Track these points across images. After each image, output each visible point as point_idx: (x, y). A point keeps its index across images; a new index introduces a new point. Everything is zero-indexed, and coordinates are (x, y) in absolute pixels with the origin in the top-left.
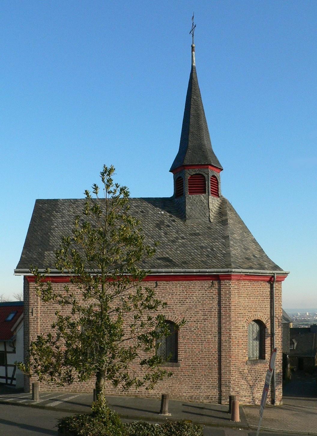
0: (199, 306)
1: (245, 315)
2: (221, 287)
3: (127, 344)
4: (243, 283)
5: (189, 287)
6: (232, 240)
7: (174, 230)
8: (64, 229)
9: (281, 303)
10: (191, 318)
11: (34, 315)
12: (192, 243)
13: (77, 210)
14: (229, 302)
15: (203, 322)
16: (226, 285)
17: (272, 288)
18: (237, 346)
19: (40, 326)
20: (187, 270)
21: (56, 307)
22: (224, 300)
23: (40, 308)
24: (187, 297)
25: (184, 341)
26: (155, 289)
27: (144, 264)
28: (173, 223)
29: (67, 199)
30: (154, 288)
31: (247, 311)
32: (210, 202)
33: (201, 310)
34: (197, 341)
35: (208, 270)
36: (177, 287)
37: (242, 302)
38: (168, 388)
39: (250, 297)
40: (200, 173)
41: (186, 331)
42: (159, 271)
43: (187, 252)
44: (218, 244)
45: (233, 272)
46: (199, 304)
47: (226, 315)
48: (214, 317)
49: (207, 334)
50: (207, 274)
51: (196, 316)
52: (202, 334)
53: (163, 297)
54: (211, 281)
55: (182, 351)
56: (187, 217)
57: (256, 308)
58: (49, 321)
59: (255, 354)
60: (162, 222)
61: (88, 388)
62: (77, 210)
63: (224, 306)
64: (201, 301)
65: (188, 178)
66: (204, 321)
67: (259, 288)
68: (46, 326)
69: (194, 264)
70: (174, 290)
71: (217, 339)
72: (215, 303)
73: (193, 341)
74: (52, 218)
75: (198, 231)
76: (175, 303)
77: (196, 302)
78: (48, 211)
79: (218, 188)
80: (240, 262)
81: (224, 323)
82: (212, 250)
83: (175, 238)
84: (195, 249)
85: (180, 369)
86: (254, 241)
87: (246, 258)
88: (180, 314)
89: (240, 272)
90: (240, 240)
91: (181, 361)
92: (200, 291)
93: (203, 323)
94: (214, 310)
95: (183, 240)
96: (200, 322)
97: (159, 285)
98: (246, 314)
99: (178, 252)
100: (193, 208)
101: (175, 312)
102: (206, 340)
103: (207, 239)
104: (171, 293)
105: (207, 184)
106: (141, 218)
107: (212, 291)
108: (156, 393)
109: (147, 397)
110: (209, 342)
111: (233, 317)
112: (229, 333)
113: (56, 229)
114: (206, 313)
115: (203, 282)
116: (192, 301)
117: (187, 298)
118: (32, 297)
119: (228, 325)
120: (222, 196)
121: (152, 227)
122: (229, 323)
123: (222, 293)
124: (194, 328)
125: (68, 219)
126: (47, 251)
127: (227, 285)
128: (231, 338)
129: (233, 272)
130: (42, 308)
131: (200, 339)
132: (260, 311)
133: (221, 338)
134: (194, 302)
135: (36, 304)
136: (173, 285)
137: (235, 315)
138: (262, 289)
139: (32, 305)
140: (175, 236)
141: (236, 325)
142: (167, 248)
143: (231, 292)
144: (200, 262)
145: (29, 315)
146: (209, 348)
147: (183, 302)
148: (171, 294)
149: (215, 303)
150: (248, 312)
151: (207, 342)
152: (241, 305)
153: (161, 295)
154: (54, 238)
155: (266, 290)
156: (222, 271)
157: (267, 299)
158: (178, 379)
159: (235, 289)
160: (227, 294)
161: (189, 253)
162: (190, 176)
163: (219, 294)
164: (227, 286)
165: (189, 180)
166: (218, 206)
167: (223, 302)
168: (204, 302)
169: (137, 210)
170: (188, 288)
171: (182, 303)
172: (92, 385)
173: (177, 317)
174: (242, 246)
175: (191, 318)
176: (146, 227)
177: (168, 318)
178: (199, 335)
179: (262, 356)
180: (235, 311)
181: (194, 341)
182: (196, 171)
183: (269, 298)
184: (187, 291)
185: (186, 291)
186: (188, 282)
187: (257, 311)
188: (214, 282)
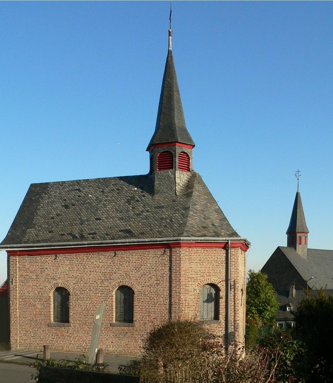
0: (152, 272)
1: (197, 280)
2: (172, 254)
3: (90, 307)
4: (195, 250)
5: (144, 255)
6: (192, 211)
7: (141, 205)
8: (48, 209)
9: (237, 267)
10: (145, 283)
11: (13, 285)
12: (155, 215)
13: (62, 191)
14: (179, 267)
15: (156, 286)
16: (177, 252)
17: (227, 254)
18: (187, 308)
19: (19, 294)
20: (140, 240)
21: (31, 277)
22: (175, 266)
23: (19, 278)
24: (142, 264)
25: (139, 304)
26: (114, 258)
27: (106, 237)
28: (143, 198)
29: (57, 182)
30: (113, 257)
31: (200, 275)
32: (176, 177)
33: (154, 275)
34: (151, 303)
35: (159, 239)
36: (133, 256)
37: (194, 268)
38: (124, 346)
39: (202, 262)
40: (169, 150)
41: (140, 295)
42: (116, 242)
43: (148, 224)
44: (178, 215)
45: (183, 240)
46: (152, 270)
47: (176, 280)
48: (166, 282)
49: (159, 297)
50: (158, 243)
51: (149, 281)
52: (155, 297)
53: (121, 265)
54: (164, 249)
55: (137, 312)
56: (156, 191)
57: (210, 273)
58: (26, 289)
59: (210, 315)
60: (133, 198)
61: (58, 346)
62: (62, 191)
63: (174, 272)
64: (154, 268)
65: (158, 156)
66: (157, 286)
67: (213, 254)
68: (24, 294)
69: (150, 235)
70: (131, 259)
71: (168, 302)
72: (167, 269)
73: (147, 304)
74: (40, 199)
75: (163, 204)
76: (132, 270)
77: (150, 269)
78: (38, 194)
79: (189, 163)
80: (194, 230)
81: (175, 287)
82: (171, 221)
83: (140, 211)
84: (156, 221)
85: (135, 329)
86: (219, 211)
87: (203, 227)
88: (136, 280)
89: (190, 240)
90: (202, 210)
91: (136, 322)
92: (154, 259)
93: (156, 287)
94: (166, 275)
95: (148, 213)
96: (153, 287)
97: (117, 255)
98: (199, 279)
99: (140, 224)
100: (161, 183)
101: (131, 278)
102: (159, 302)
103: (169, 211)
104: (128, 261)
105: (174, 160)
106: (116, 195)
107: (164, 258)
108: (114, 351)
109: (107, 354)
110: (160, 305)
111: (183, 281)
112: (179, 296)
113: (42, 209)
114: (159, 278)
115: (156, 250)
116: (146, 268)
117: (142, 265)
118: (12, 269)
119: (178, 289)
120: (193, 170)
121: (123, 202)
122: (179, 287)
123: (172, 260)
124: (147, 292)
125: (53, 200)
126: (29, 228)
127: (178, 252)
128: (180, 301)
129: (183, 240)
130: (21, 278)
131: (153, 301)
132: (214, 276)
133: (171, 301)
134: (148, 269)
135: (15, 275)
136: (130, 254)
137: (185, 279)
138: (216, 255)
139: (12, 275)
140: (141, 210)
141: (186, 288)
142: (131, 221)
143: (181, 259)
144: (156, 232)
145: (10, 284)
146: (161, 310)
147: (138, 269)
148: (128, 262)
149: (167, 269)
150: (201, 276)
151: (159, 304)
152: (193, 270)
153: (119, 263)
154: (37, 217)
155: (221, 256)
156: (171, 239)
157: (222, 264)
158: (134, 338)
159: (185, 255)
160: (177, 260)
161: (149, 225)
162: (160, 154)
163: (171, 261)
164: (177, 253)
165: (158, 157)
166: (188, 180)
167: (173, 268)
168: (157, 268)
169: (114, 188)
170: (143, 256)
171: (137, 270)
172: (61, 343)
173: (133, 282)
174: (202, 216)
175: (145, 283)
176: (118, 203)
177: (125, 284)
178: (153, 298)
179: (216, 317)
180: (185, 276)
181: (147, 303)
182: (165, 148)
183: (224, 264)
184: (142, 259)
185: (141, 259)
186: (143, 251)
187: (211, 276)
188: (166, 250)
